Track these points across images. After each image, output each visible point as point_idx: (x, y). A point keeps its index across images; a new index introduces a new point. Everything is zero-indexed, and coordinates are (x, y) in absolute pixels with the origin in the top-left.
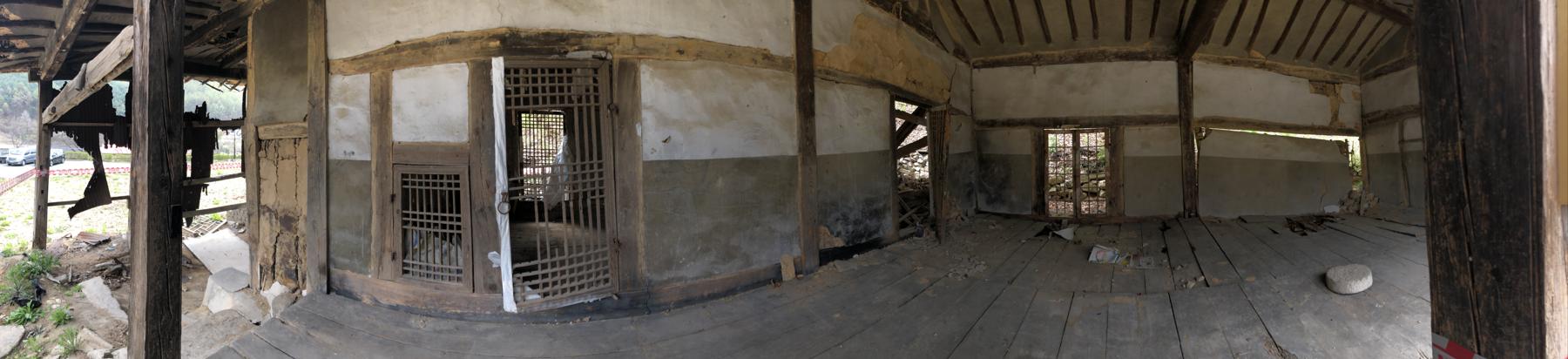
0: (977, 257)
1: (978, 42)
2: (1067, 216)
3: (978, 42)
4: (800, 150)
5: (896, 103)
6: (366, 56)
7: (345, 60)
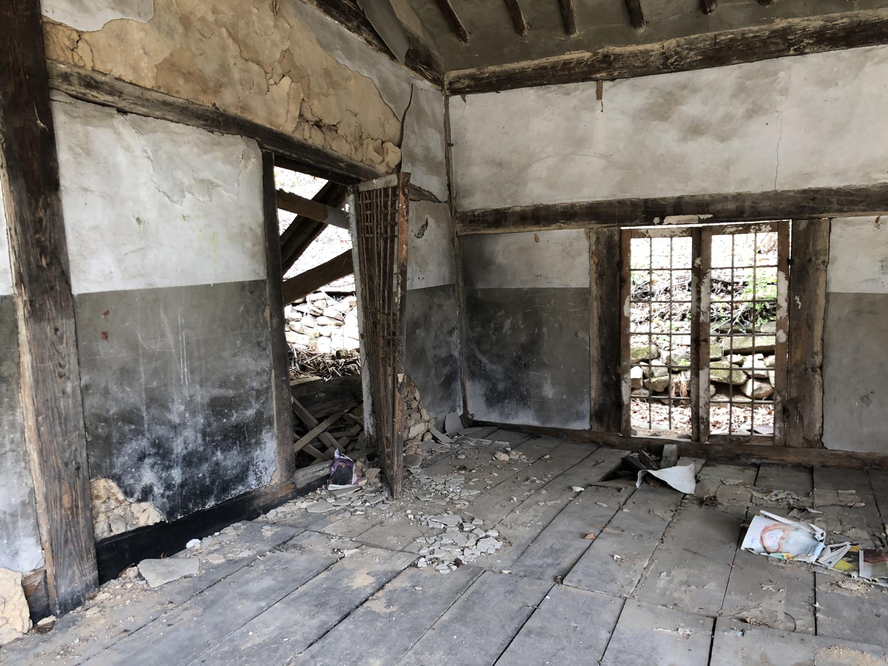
0: (478, 522)
1: (461, 35)
2: (674, 437)
3: (461, 35)
4: (20, 280)
5: (277, 170)
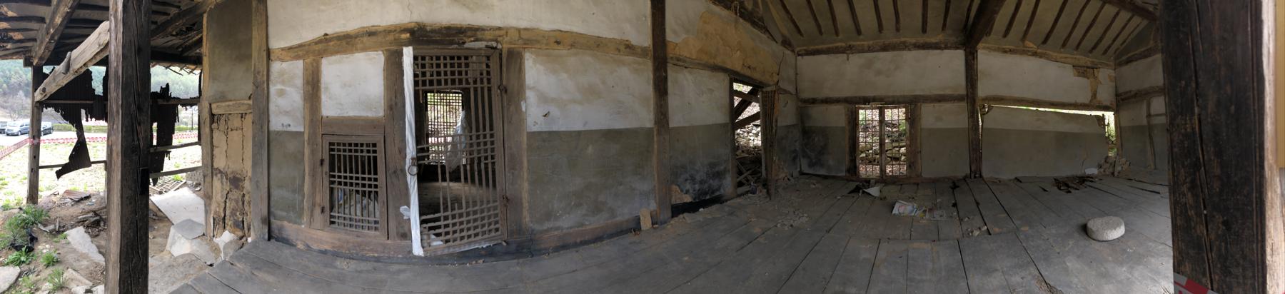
1: (802, 35)
2: (874, 177)
3: (802, 35)
4: (656, 123)
5: (735, 84)
6: (300, 46)
7: (283, 49)
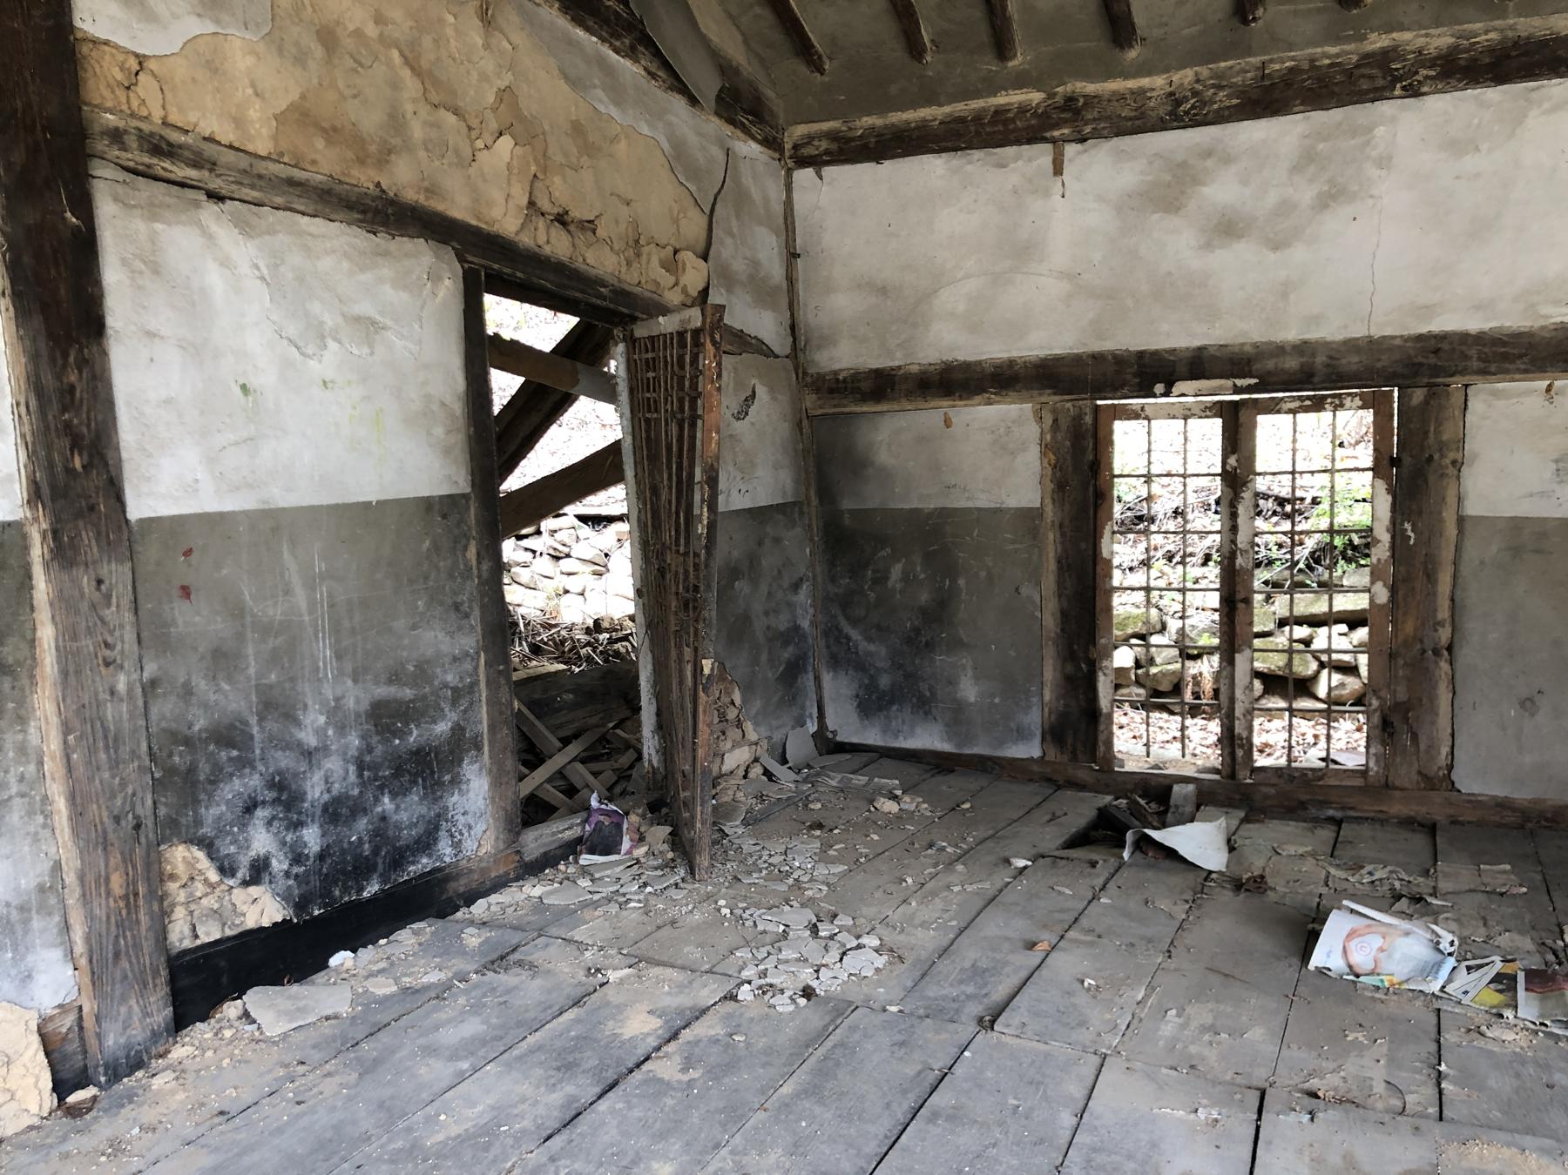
1: (814, 63)
2: (1190, 772)
3: (814, 63)
4: (35, 495)
5: (489, 300)
